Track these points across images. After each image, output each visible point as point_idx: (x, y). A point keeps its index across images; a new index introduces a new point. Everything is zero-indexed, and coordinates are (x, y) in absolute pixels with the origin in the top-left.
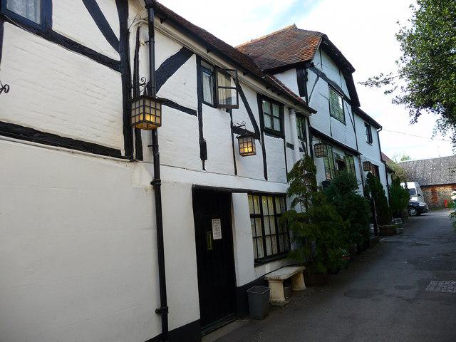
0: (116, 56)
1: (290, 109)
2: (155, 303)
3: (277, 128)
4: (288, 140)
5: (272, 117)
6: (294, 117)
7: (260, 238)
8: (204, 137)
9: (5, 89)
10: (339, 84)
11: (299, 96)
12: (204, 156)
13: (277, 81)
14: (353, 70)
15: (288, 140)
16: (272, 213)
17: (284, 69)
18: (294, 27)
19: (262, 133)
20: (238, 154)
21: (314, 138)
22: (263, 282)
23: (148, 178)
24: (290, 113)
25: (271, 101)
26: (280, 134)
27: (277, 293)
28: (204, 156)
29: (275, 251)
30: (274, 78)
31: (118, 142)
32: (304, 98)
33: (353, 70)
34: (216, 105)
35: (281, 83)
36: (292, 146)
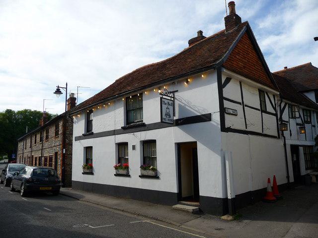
0: (274, 112)
1: (313, 111)
2: (285, 175)
3: (309, 120)
5: (307, 116)
6: (315, 115)
7: (306, 161)
9: (316, 39)
12: (291, 135)
14: (311, 63)
17: (308, 91)
20: (299, 133)
22: (308, 175)
24: (313, 113)
25: (306, 110)
26: (310, 122)
27: (314, 179)
28: (291, 135)
29: (310, 166)
31: (276, 135)
33: (311, 63)
34: (292, 118)
35: (307, 97)
36: (314, 126)
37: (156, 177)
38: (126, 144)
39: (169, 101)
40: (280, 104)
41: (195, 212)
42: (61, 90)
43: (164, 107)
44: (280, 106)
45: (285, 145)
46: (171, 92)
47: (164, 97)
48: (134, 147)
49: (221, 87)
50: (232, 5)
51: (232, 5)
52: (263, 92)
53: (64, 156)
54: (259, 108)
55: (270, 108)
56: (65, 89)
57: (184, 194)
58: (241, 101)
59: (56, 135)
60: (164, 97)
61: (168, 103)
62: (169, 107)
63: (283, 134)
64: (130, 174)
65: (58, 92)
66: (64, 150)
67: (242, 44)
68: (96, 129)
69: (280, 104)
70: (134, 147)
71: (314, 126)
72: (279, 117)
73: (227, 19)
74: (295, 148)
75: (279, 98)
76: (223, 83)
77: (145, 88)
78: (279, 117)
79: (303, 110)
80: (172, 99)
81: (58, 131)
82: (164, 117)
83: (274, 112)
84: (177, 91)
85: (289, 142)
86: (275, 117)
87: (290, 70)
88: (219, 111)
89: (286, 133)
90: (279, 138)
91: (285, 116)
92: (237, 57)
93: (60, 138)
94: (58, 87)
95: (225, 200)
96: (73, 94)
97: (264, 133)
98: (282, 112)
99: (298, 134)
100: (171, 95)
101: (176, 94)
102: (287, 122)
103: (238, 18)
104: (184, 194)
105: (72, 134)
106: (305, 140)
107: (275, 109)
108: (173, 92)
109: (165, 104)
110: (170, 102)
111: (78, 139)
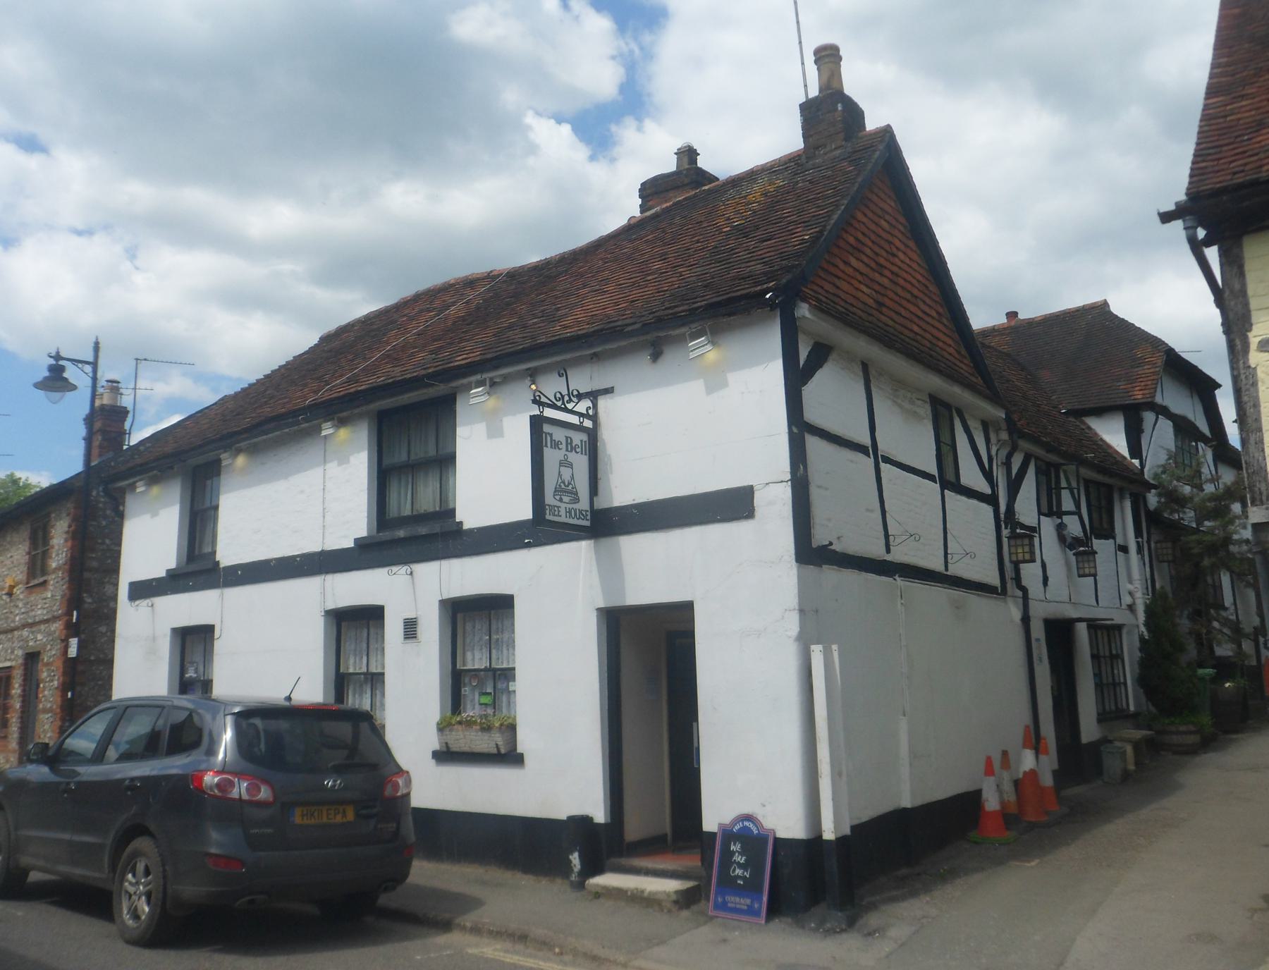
0: (984, 488)
1: (1121, 490)
4: (1120, 540)
8: (1044, 558)
10: (1191, 416)
11: (1129, 458)
12: (12, 455)
13: (1089, 428)
15: (1120, 540)
16: (1107, 654)
17: (1100, 412)
18: (1105, 304)
19: (1091, 536)
21: (1153, 530)
23: (1016, 614)
26: (1109, 534)
30: (1085, 423)
31: (993, 579)
32: (1136, 462)
37: (510, 757)
38: (370, 616)
39: (571, 433)
40: (1009, 456)
41: (687, 900)
42: (71, 373)
43: (551, 457)
44: (1007, 464)
45: (1026, 620)
46: (580, 397)
47: (549, 413)
48: (410, 628)
49: (796, 378)
50: (828, 57)
51: (828, 57)
52: (948, 406)
53: (71, 667)
54: (933, 469)
55: (971, 476)
56: (88, 369)
57: (634, 830)
58: (867, 441)
59: (32, 573)
60: (549, 413)
61: (569, 441)
62: (572, 457)
63: (1017, 579)
64: (525, 741)
65: (55, 379)
66: (74, 642)
67: (870, 214)
68: (229, 552)
69: (1009, 456)
70: (410, 628)
71: (1124, 549)
72: (1003, 508)
73: (811, 111)
74: (1059, 631)
75: (1004, 436)
76: (802, 363)
77: (472, 368)
78: (1003, 508)
79: (1088, 483)
80: (588, 424)
81: (45, 555)
82: (549, 499)
83: (984, 488)
84: (608, 391)
85: (1039, 611)
86: (987, 510)
87: (1031, 323)
88: (788, 477)
89: (1031, 573)
90: (1004, 592)
91: (1027, 507)
92: (854, 262)
93: (55, 590)
94: (58, 357)
95: (814, 844)
96: (114, 386)
97: (954, 570)
98: (1014, 487)
99: (1069, 576)
100: (583, 406)
101: (603, 402)
102: (1033, 529)
103: (854, 114)
104: (634, 830)
105: (114, 570)
106: (1095, 604)
107: (988, 475)
108: (594, 395)
109: (556, 445)
110: (578, 438)
111: (142, 590)
